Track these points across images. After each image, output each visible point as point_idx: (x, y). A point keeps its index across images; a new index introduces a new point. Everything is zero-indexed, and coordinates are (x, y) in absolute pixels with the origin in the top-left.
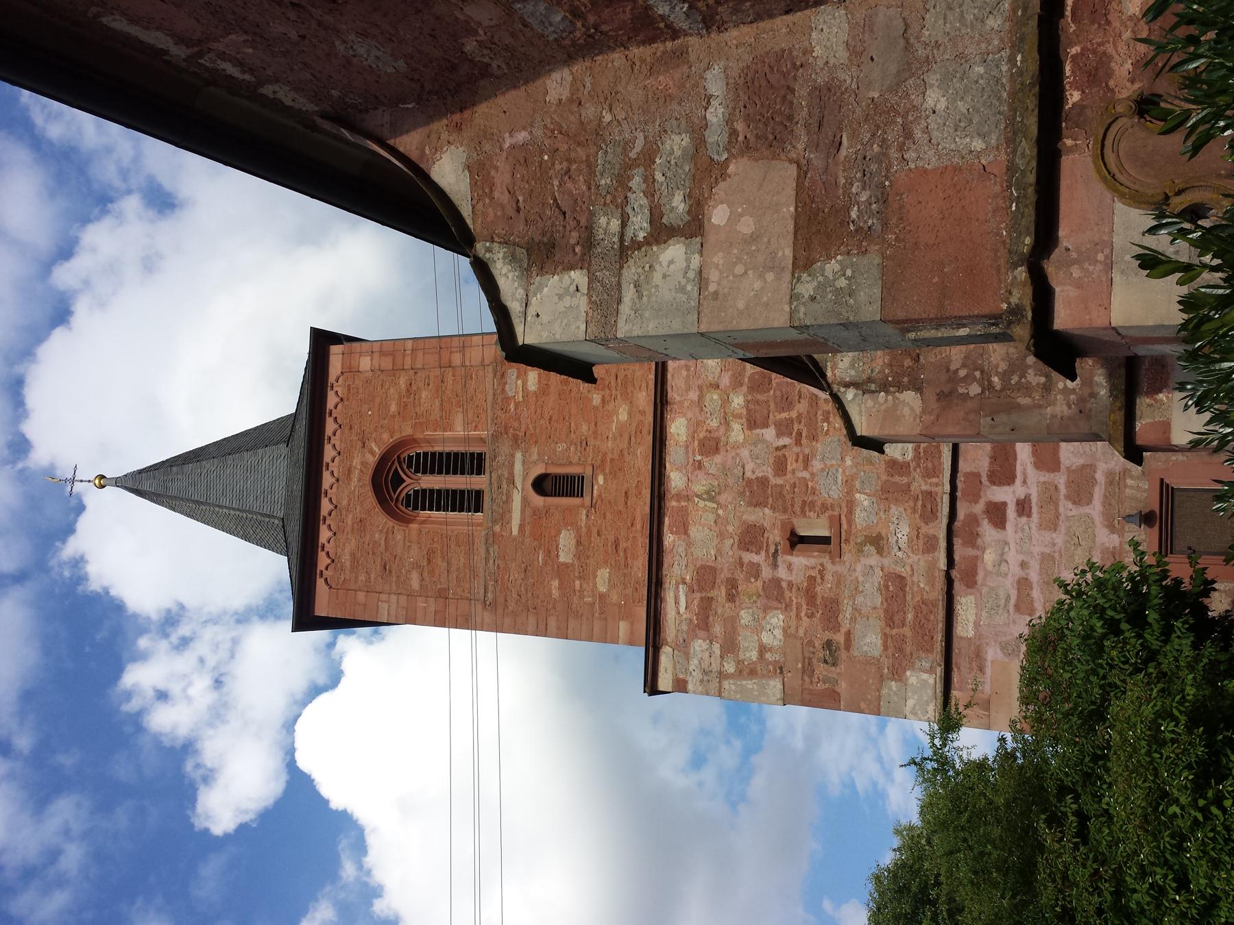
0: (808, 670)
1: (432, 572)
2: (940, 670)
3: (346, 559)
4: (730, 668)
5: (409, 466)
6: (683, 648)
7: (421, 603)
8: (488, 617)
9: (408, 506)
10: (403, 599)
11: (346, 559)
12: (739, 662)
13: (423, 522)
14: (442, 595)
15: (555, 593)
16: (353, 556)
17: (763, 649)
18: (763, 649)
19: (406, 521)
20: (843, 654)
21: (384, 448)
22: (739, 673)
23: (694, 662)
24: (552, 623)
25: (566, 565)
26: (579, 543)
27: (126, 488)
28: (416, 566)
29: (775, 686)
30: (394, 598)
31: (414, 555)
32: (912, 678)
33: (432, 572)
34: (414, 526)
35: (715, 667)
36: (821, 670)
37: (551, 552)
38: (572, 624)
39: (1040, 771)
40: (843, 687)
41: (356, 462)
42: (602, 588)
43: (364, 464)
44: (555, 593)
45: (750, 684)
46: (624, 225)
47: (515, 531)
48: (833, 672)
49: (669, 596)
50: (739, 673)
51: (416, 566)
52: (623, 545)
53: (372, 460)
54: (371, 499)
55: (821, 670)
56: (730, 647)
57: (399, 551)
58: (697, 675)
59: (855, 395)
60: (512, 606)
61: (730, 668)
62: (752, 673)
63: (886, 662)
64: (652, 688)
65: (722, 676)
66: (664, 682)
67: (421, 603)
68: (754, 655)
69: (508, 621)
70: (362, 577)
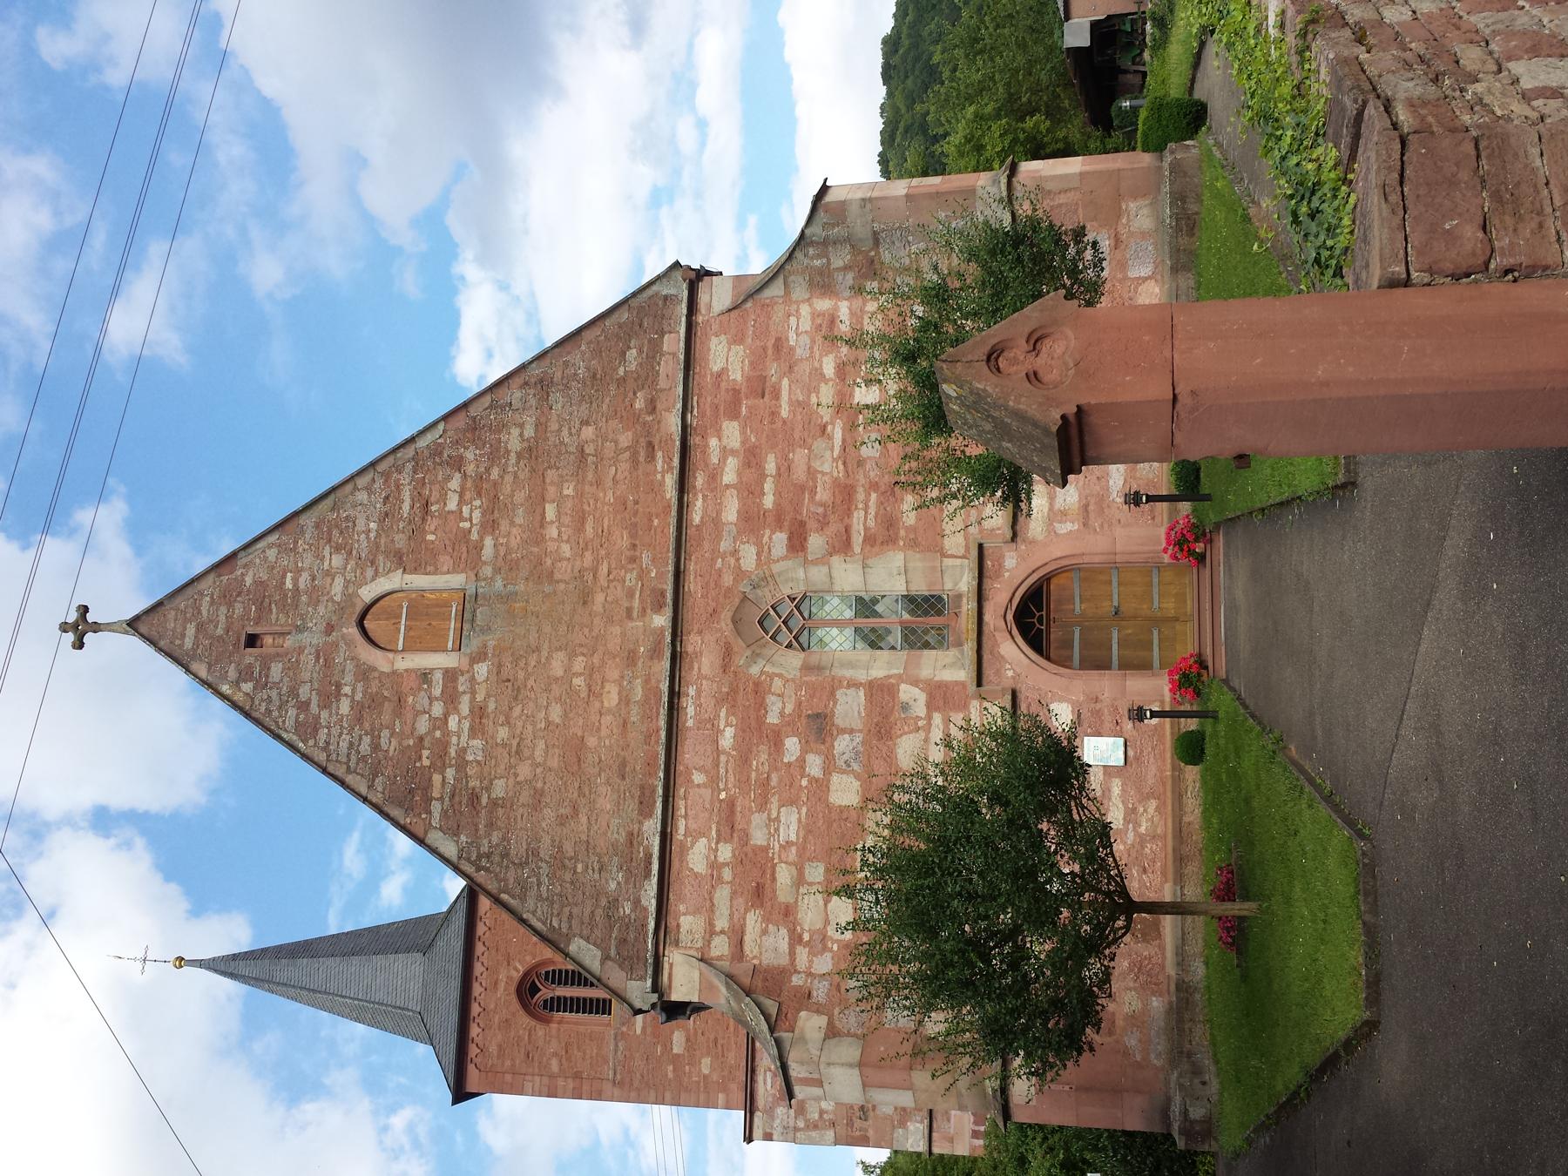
0: (850, 1124)
1: (569, 1059)
2: (926, 1122)
3: (493, 1049)
4: (801, 1124)
5: (547, 979)
6: (770, 1113)
7: (561, 1082)
8: (617, 1092)
9: (545, 1007)
10: (546, 1080)
11: (493, 1049)
12: (806, 1121)
13: (560, 1022)
14: (577, 1076)
15: (670, 1075)
16: (500, 1046)
17: (822, 1112)
18: (822, 1112)
19: (546, 1021)
20: (871, 1114)
21: (527, 966)
22: (807, 1127)
23: (778, 1122)
24: (668, 1095)
25: (678, 1055)
26: (688, 1040)
27: (216, 971)
28: (555, 1054)
29: (830, 1134)
30: (537, 1079)
31: (554, 1046)
32: (911, 1126)
33: (569, 1059)
34: (554, 1026)
35: (792, 1124)
36: (858, 1123)
37: (668, 1046)
38: (683, 1095)
40: (871, 1133)
41: (502, 977)
42: (706, 1071)
43: (510, 978)
44: (670, 1075)
45: (814, 1134)
47: (639, 1031)
48: (865, 1124)
49: (760, 1078)
50: (807, 1127)
51: (555, 1054)
52: (720, 1042)
53: (517, 976)
54: (515, 1004)
55: (858, 1123)
56: (801, 1111)
57: (541, 1043)
58: (780, 1129)
59: (479, 485)
60: (636, 1084)
61: (801, 1124)
62: (816, 1127)
63: (896, 1118)
64: (749, 1139)
65: (796, 1129)
66: (757, 1132)
67: (561, 1082)
68: (816, 1116)
69: (633, 1094)
70: (508, 1063)
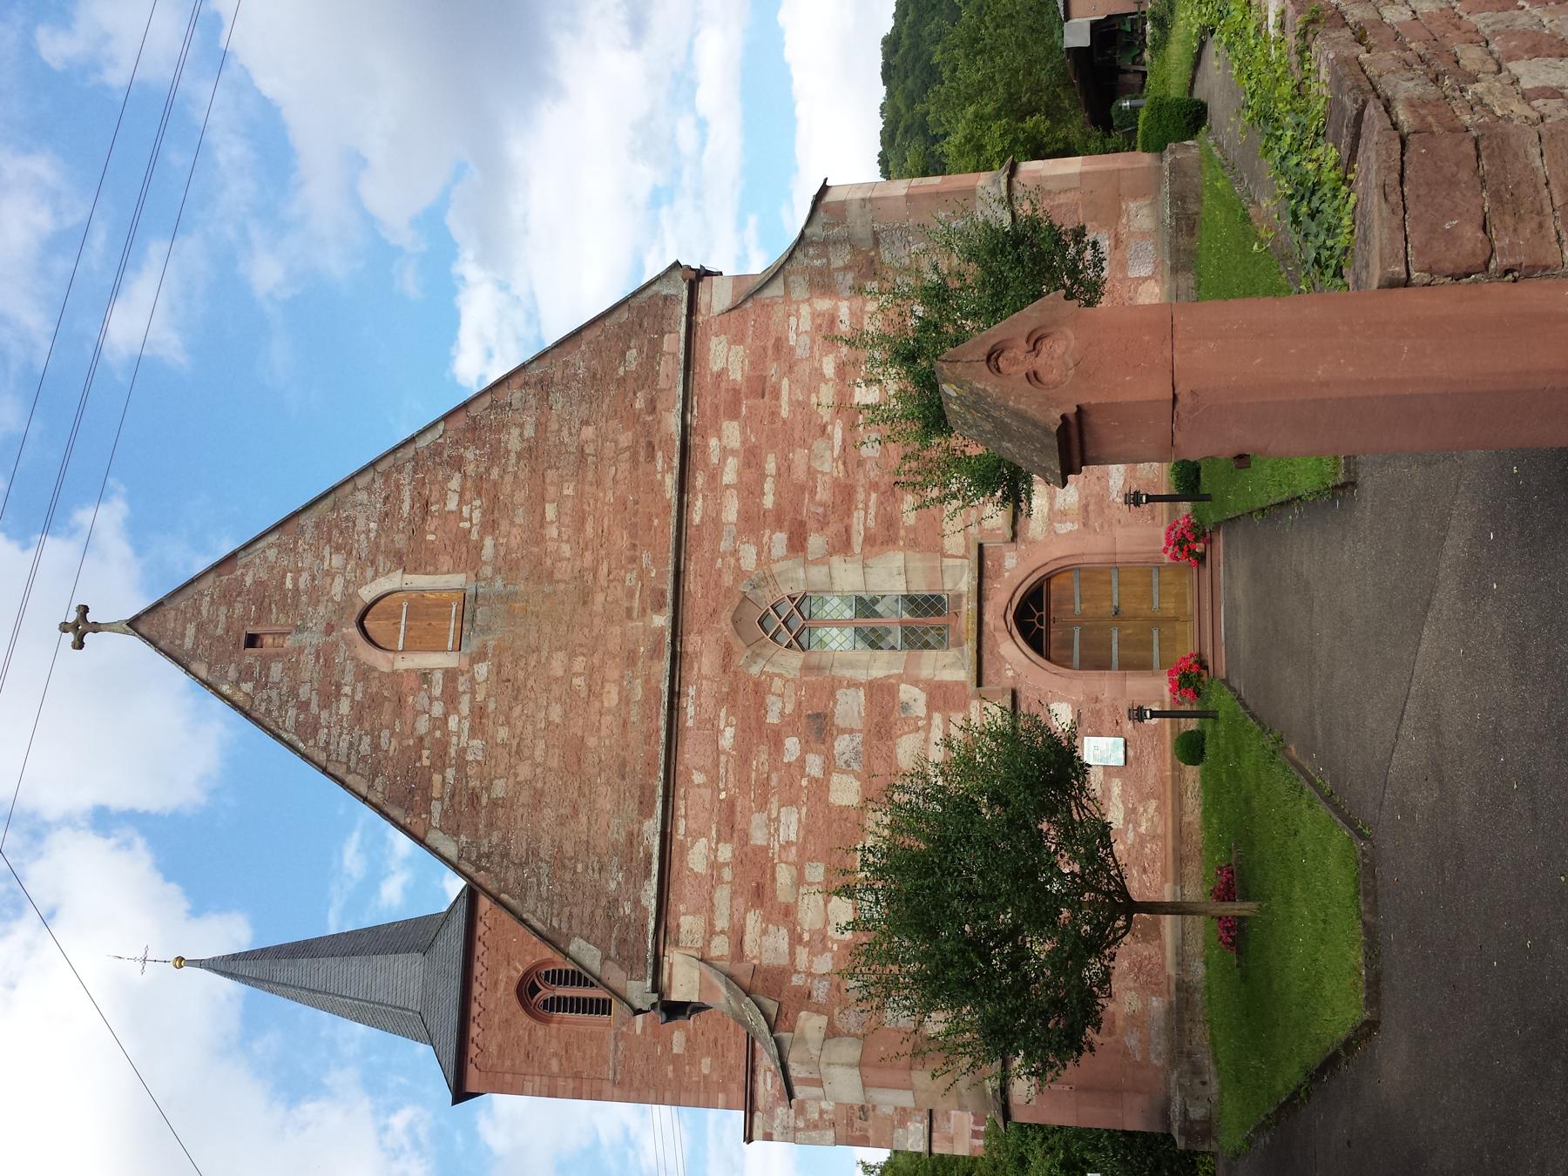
0: (850, 1124)
1: (569, 1059)
2: (926, 1122)
3: (493, 1049)
4: (801, 1124)
5: (547, 979)
6: (770, 1113)
7: (561, 1082)
8: (617, 1092)
9: (545, 1007)
10: (546, 1080)
11: (493, 1049)
12: (806, 1121)
13: (560, 1022)
14: (577, 1076)
15: (670, 1075)
16: (500, 1046)
17: (822, 1112)
18: (822, 1112)
19: (546, 1021)
20: (871, 1114)
21: (527, 966)
22: (807, 1127)
23: (778, 1122)
24: (668, 1095)
25: (678, 1055)
26: (688, 1040)
27: (216, 971)
28: (555, 1054)
29: (830, 1134)
30: (537, 1079)
31: (554, 1046)
32: (911, 1126)
33: (569, 1059)
34: (554, 1026)
35: (792, 1124)
36: (858, 1123)
37: (668, 1046)
38: (683, 1095)
40: (871, 1133)
41: (502, 977)
42: (706, 1071)
43: (510, 978)
44: (670, 1075)
45: (814, 1134)
46: (1004, 1091)
47: (639, 1031)
48: (865, 1124)
49: (760, 1078)
50: (807, 1127)
51: (555, 1054)
52: (720, 1042)
53: (517, 976)
54: (515, 1004)
55: (858, 1123)
56: (801, 1111)
57: (541, 1043)
58: (780, 1129)
59: (479, 485)
60: (636, 1084)
61: (801, 1124)
62: (816, 1127)
63: (896, 1118)
64: (749, 1139)
65: (796, 1129)
66: (757, 1132)
67: (561, 1082)
68: (816, 1116)
69: (633, 1094)
70: (508, 1063)
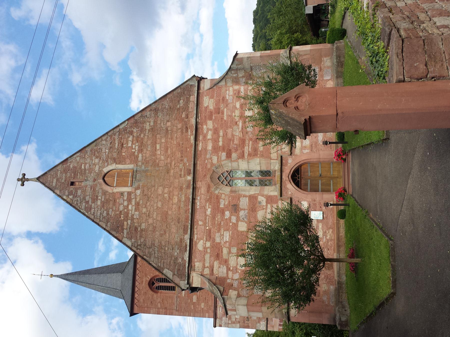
0: (244, 322)
1: (163, 304)
2: (266, 321)
3: (142, 301)
4: (230, 322)
5: (157, 280)
6: (221, 319)
7: (161, 310)
8: (177, 313)
9: (156, 289)
10: (157, 310)
11: (142, 301)
12: (231, 321)
13: (161, 293)
14: (166, 308)
15: (192, 308)
16: (143, 300)
17: (236, 319)
18: (236, 319)
19: (157, 293)
20: (250, 319)
21: (151, 277)
22: (232, 323)
23: (223, 321)
24: (192, 314)
25: (195, 302)
26: (197, 298)
27: (62, 278)
28: (159, 302)
29: (238, 325)
30: (154, 309)
31: (159, 300)
32: (261, 323)
33: (163, 304)
34: (159, 294)
35: (227, 322)
36: (246, 322)
37: (192, 300)
38: (196, 314)
39: (264, 281)
40: (250, 325)
41: (144, 280)
42: (203, 307)
43: (146, 280)
44: (192, 308)
45: (233, 325)
47: (183, 296)
48: (248, 322)
49: (218, 309)
50: (232, 323)
51: (159, 302)
52: (207, 298)
53: (148, 280)
54: (148, 288)
55: (246, 322)
56: (230, 318)
57: (155, 299)
58: (224, 324)
60: (183, 311)
61: (230, 322)
62: (234, 323)
63: (257, 320)
64: (215, 326)
65: (228, 324)
66: (217, 324)
67: (161, 310)
68: (234, 320)
69: (182, 314)
70: (146, 305)
